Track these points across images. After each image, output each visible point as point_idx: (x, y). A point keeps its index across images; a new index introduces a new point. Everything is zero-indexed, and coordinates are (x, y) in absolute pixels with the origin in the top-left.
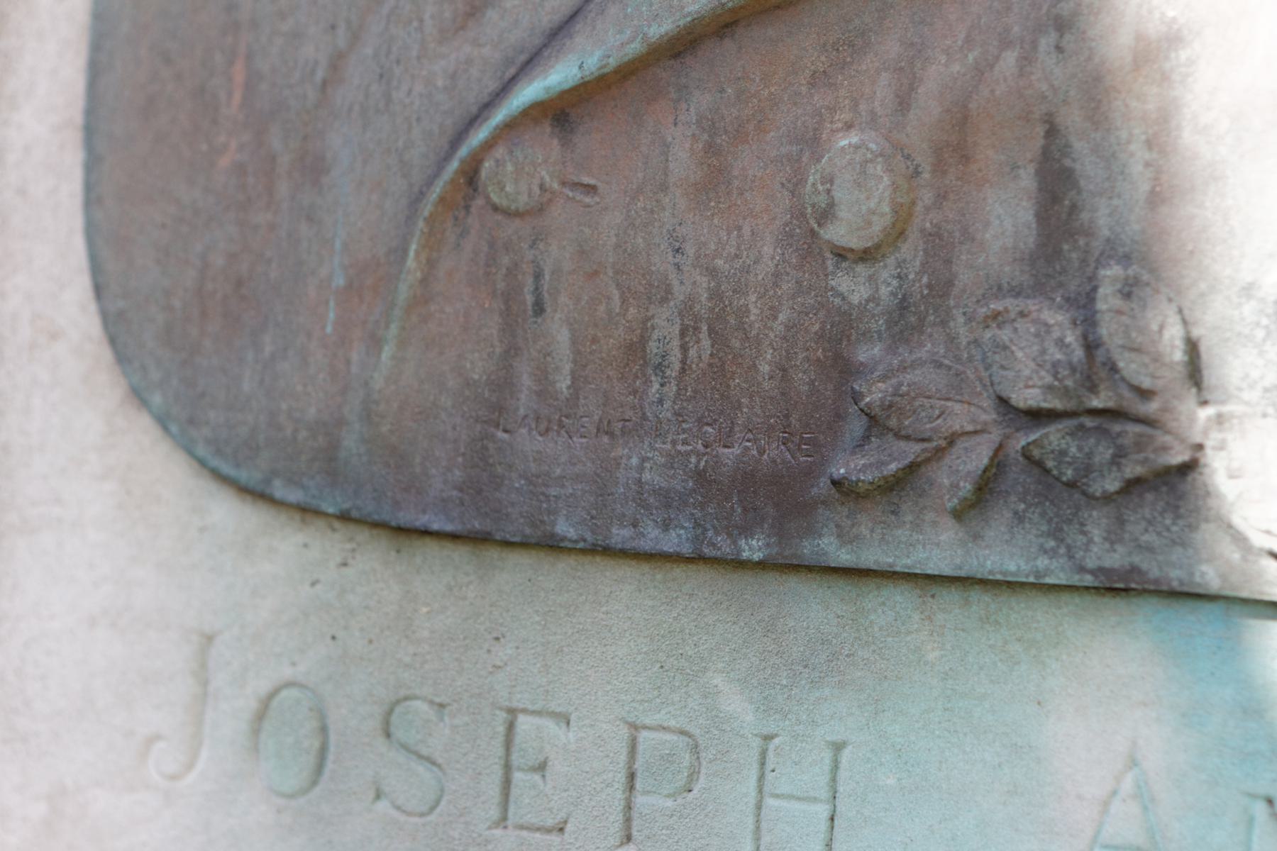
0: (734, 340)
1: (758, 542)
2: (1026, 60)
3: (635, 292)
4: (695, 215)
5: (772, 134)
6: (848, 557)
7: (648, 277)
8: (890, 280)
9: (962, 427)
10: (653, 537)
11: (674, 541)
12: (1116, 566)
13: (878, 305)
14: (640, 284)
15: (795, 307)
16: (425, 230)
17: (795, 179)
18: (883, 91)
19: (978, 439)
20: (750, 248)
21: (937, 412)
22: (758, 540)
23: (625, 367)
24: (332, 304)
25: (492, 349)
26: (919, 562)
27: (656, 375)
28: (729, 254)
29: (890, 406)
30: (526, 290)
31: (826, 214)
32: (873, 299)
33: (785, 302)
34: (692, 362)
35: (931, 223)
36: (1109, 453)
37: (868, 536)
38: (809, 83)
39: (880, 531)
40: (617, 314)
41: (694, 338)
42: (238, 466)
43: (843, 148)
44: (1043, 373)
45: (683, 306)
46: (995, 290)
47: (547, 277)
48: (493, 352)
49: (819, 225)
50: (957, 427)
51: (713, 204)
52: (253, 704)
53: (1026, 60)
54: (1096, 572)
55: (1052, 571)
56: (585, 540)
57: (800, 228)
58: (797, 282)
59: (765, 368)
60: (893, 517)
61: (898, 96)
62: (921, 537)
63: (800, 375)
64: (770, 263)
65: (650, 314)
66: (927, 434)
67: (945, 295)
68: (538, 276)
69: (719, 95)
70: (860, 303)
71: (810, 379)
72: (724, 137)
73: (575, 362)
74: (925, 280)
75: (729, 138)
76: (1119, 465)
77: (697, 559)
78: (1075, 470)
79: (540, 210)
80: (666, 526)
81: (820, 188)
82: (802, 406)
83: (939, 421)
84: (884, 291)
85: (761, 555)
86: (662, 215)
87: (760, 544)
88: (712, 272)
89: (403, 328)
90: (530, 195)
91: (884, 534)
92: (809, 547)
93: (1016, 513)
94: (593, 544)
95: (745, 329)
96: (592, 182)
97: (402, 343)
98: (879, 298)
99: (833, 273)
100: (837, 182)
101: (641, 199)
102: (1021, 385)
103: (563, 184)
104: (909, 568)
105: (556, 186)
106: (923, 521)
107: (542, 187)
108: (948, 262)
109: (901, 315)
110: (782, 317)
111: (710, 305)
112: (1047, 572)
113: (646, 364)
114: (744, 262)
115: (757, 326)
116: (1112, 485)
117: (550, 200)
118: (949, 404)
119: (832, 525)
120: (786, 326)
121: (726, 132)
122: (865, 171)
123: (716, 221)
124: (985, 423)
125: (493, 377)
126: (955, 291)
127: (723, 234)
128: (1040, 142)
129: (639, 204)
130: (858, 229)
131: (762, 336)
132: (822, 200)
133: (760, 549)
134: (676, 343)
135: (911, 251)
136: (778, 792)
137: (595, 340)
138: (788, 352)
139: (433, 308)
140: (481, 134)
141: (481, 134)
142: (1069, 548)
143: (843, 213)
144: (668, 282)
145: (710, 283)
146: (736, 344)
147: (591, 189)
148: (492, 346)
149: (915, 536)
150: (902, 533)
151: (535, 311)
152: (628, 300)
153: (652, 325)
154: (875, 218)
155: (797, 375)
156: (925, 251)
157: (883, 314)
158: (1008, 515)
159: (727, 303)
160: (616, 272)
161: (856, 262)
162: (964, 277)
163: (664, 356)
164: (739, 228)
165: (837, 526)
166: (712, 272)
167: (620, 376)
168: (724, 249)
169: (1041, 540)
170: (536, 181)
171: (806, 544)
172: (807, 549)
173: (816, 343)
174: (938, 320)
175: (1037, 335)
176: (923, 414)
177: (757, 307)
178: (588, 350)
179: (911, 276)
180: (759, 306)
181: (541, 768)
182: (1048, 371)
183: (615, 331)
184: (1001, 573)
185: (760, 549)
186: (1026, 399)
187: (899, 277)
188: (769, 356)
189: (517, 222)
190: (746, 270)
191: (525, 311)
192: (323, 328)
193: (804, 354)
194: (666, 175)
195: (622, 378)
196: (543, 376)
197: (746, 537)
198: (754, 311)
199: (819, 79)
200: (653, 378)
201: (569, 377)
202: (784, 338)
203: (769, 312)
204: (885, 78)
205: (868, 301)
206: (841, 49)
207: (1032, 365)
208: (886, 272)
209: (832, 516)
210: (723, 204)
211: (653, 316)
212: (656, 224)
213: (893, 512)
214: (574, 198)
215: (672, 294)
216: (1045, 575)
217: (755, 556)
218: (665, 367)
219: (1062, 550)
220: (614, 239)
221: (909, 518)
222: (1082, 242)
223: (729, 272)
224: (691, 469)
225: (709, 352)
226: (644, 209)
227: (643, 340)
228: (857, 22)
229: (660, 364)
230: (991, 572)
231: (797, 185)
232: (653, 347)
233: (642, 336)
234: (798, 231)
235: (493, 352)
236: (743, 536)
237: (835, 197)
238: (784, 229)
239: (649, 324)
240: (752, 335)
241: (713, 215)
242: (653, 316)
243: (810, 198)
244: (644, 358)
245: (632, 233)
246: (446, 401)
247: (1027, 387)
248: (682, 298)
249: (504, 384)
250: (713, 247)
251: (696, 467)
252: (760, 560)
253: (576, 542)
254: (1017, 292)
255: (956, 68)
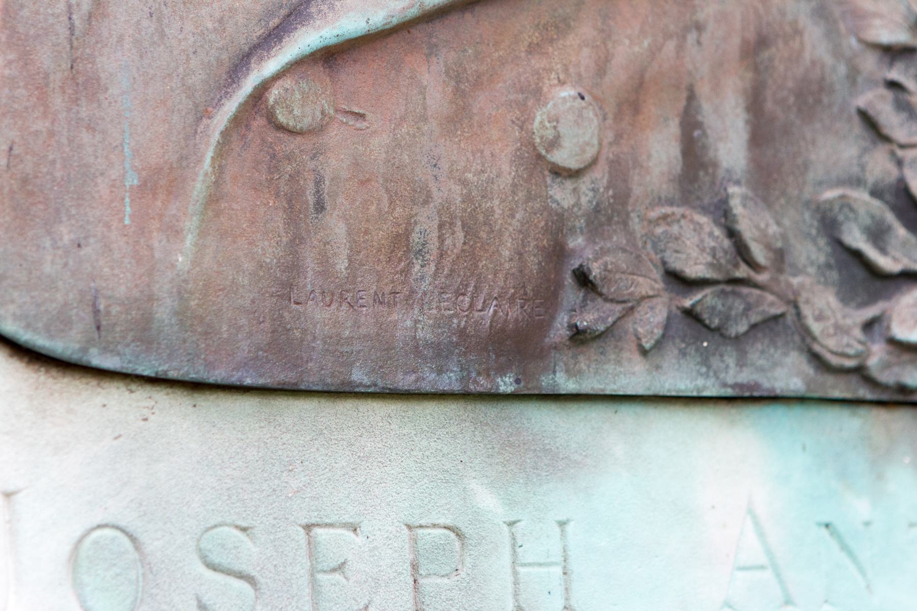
0: (482, 232)
1: (509, 379)
2: (680, 48)
3: (401, 196)
4: (446, 140)
5: (500, 85)
6: (574, 386)
7: (412, 185)
8: (587, 192)
9: (647, 292)
10: (430, 380)
11: (450, 381)
12: (745, 381)
13: (580, 209)
14: (405, 190)
15: (527, 209)
16: (221, 142)
17: (523, 118)
18: (585, 58)
19: (655, 300)
20: (492, 166)
21: (630, 282)
22: (510, 377)
23: (391, 253)
24: (127, 200)
25: (279, 239)
26: (622, 387)
27: (417, 259)
28: (476, 170)
29: (605, 278)
30: (308, 192)
31: (554, 143)
32: (577, 204)
33: (520, 205)
34: (448, 249)
35: (613, 154)
36: (742, 307)
37: (587, 371)
38: (526, 51)
39: (594, 366)
40: (386, 213)
41: (450, 231)
42: (51, 337)
43: (564, 98)
44: (705, 255)
45: (440, 207)
46: (657, 200)
47: (327, 183)
48: (281, 241)
49: (547, 151)
50: (644, 293)
51: (459, 133)
52: (67, 548)
53: (680, 48)
54: (735, 386)
55: (708, 388)
56: (375, 385)
57: (528, 153)
58: (528, 191)
59: (506, 253)
60: (603, 357)
61: (597, 65)
62: (622, 370)
63: (532, 258)
64: (508, 177)
65: (413, 213)
66: (626, 298)
67: (624, 204)
68: (318, 182)
69: (462, 54)
70: (569, 208)
71: (539, 261)
72: (466, 84)
73: (351, 249)
74: (611, 193)
75: (470, 85)
76: (747, 317)
77: (465, 396)
78: (720, 319)
79: (317, 130)
80: (440, 371)
81: (548, 125)
82: (534, 280)
83: (632, 289)
84: (584, 200)
85: (513, 389)
86: (422, 139)
87: (511, 380)
88: (464, 183)
89: (203, 221)
90: (313, 119)
91: (597, 369)
92: (545, 381)
93: (680, 350)
94: (383, 388)
95: (490, 224)
96: (361, 111)
97: (203, 233)
98: (581, 205)
99: (552, 187)
100: (562, 121)
101: (405, 126)
102: (692, 263)
103: (336, 111)
104: (615, 391)
105: (332, 112)
106: (622, 358)
107: (323, 113)
108: (625, 181)
109: (596, 217)
110: (518, 216)
111: (463, 206)
112: (705, 388)
113: (408, 250)
114: (489, 176)
115: (500, 222)
116: (742, 328)
117: (328, 123)
118: (635, 277)
119: (561, 364)
120: (521, 223)
121: (468, 81)
122: (582, 115)
123: (462, 145)
124: (658, 290)
125: (282, 261)
126: (631, 200)
127: (469, 155)
128: (683, 103)
129: (403, 130)
130: (576, 155)
131: (503, 229)
132: (550, 134)
133: (511, 384)
134: (435, 234)
135: (600, 174)
136: (526, 562)
137: (366, 232)
138: (523, 241)
139: (223, 205)
140: (271, 66)
141: (271, 66)
142: (715, 373)
143: (566, 143)
144: (428, 189)
145: (462, 190)
146: (483, 235)
147: (362, 116)
148: (279, 236)
149: (618, 369)
150: (610, 367)
151: (316, 209)
152: (395, 202)
153: (415, 221)
154: (588, 148)
155: (529, 258)
156: (610, 173)
157: (584, 216)
158: (676, 352)
159: (477, 205)
160: (386, 180)
161: (565, 178)
162: (637, 191)
163: (424, 244)
164: (482, 152)
165: (566, 365)
166: (464, 183)
167: (388, 259)
168: (471, 166)
169: (698, 367)
170: (319, 108)
171: (543, 378)
172: (546, 383)
173: (543, 235)
174: (620, 220)
175: (695, 230)
176: (622, 284)
177: (500, 208)
178: (362, 240)
179: (602, 190)
180: (502, 208)
181: (340, 568)
182: (708, 254)
183: (384, 226)
184: (675, 391)
185: (511, 384)
186: (696, 273)
187: (593, 190)
188: (509, 244)
189: (299, 139)
190: (491, 181)
191: (307, 209)
192: (121, 220)
193: (535, 243)
194: (425, 109)
195: (389, 261)
196: (325, 261)
197: (501, 378)
198: (498, 211)
199: (533, 49)
200: (414, 261)
201: (346, 261)
202: (520, 232)
203: (508, 212)
204: (586, 51)
205: (573, 206)
206: (549, 29)
207: (696, 249)
208: (584, 184)
209: (561, 357)
210: (467, 133)
211: (416, 215)
212: (418, 145)
213: (601, 353)
214: (346, 123)
215: (431, 198)
216: (703, 391)
217: (508, 389)
218: (425, 252)
219: (711, 374)
220: (384, 155)
221: (613, 357)
222: (710, 170)
223: (478, 183)
224: (454, 328)
225: (462, 241)
226: (408, 134)
227: (407, 233)
228: (560, 11)
229: (420, 250)
230: (669, 390)
231: (525, 122)
232: (415, 237)
233: (406, 229)
234: (526, 155)
235: (281, 241)
236: (498, 376)
237: (560, 132)
238: (516, 153)
239: (413, 220)
240: (496, 229)
241: (460, 141)
242: (416, 215)
243: (538, 131)
244: (407, 246)
245: (399, 151)
246: (243, 280)
247: (696, 264)
248: (440, 201)
249: (294, 267)
250: (463, 164)
251: (458, 326)
252: (512, 392)
253: (369, 386)
254: (671, 202)
255: (637, 49)
